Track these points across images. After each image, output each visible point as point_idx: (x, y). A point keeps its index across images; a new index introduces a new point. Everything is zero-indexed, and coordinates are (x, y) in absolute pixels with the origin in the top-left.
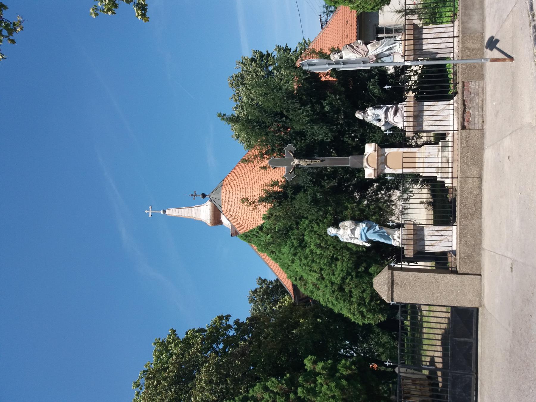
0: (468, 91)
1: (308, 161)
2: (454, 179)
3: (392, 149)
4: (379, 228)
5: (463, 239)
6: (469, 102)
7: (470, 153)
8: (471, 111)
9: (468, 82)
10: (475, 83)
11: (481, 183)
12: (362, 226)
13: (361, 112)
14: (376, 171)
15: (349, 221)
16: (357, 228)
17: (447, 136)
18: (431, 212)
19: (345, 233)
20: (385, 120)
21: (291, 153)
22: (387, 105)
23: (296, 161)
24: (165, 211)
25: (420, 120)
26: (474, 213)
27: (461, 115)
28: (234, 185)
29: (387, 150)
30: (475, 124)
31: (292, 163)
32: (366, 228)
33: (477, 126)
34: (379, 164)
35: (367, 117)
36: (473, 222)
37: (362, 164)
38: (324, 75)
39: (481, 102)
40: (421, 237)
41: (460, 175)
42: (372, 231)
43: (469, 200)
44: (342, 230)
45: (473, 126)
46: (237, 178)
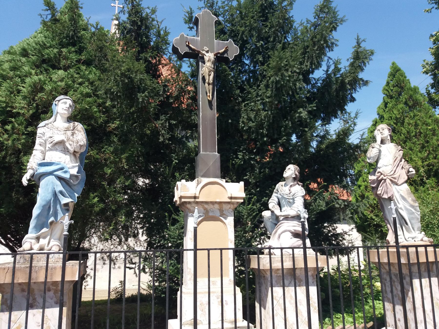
1: (211, 77)
4: (66, 205)
12: (74, 167)
13: (297, 174)
14: (193, 200)
19: (56, 132)
21: (223, 50)
23: (210, 56)
25: (285, 280)
29: (230, 221)
31: (206, 49)
32: (67, 176)
34: (206, 206)
37: (204, 176)
40: (40, 300)
42: (59, 187)
44: (66, 125)
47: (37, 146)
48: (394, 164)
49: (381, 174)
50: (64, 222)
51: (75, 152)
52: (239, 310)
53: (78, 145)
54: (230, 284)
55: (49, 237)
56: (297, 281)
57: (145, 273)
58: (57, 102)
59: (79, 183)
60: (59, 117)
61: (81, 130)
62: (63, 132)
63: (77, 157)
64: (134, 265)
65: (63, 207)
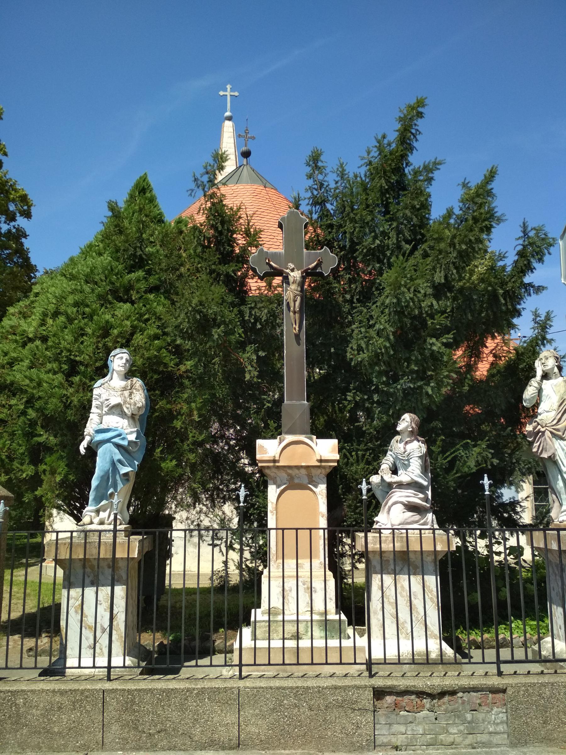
0: (480, 705)
1: (298, 303)
2: (243, 663)
3: (326, 502)
4: (126, 474)
5: (65, 700)
6: (450, 708)
7: (308, 713)
8: (425, 712)
9: (505, 705)
10: (502, 722)
11: (223, 748)
12: (132, 433)
13: (414, 426)
14: (272, 464)
15: (143, 400)
16: (126, 421)
17: (354, 629)
18: (205, 583)
19: (112, 393)
20: (395, 483)
22: (430, 487)
23: (296, 275)
24: (229, 119)
26: (140, 729)
27: (414, 686)
28: (265, 206)
29: (322, 489)
30: (390, 724)
31: (291, 266)
32: (125, 443)
33: (384, 732)
34: (290, 471)
35: (401, 441)
36: (115, 728)
37: (290, 432)
38: (494, 351)
39: (450, 739)
41: (245, 688)
42: (118, 456)
43: (175, 715)
44: (123, 383)
45: (382, 720)
46: (279, 211)
47: (94, 409)
48: (558, 409)
49: (538, 424)
50: (114, 501)
51: (132, 414)
52: (331, 599)
53: (136, 407)
54: (320, 567)
55: (109, 510)
56: (411, 568)
57: (234, 549)
58: (112, 357)
59: (139, 449)
60: (115, 375)
61: (140, 388)
62: (120, 393)
63: (137, 420)
64: (220, 541)
65: (122, 477)
